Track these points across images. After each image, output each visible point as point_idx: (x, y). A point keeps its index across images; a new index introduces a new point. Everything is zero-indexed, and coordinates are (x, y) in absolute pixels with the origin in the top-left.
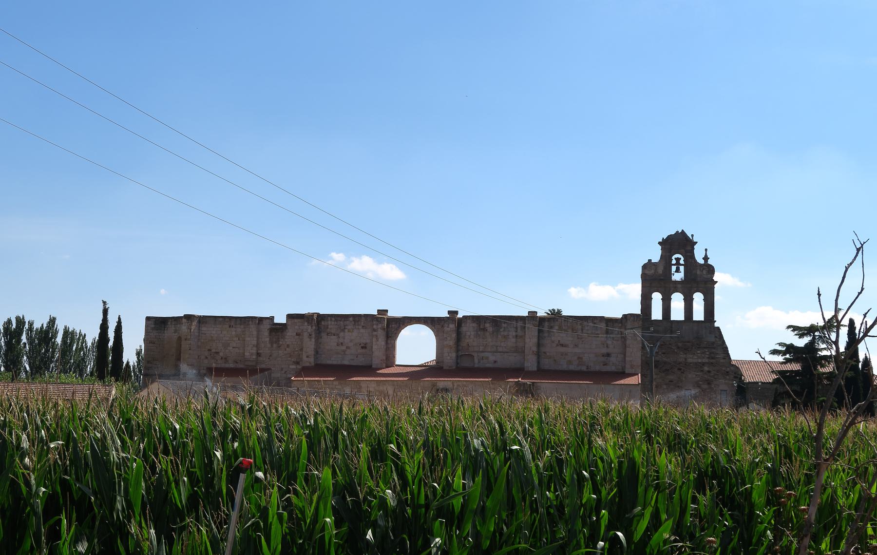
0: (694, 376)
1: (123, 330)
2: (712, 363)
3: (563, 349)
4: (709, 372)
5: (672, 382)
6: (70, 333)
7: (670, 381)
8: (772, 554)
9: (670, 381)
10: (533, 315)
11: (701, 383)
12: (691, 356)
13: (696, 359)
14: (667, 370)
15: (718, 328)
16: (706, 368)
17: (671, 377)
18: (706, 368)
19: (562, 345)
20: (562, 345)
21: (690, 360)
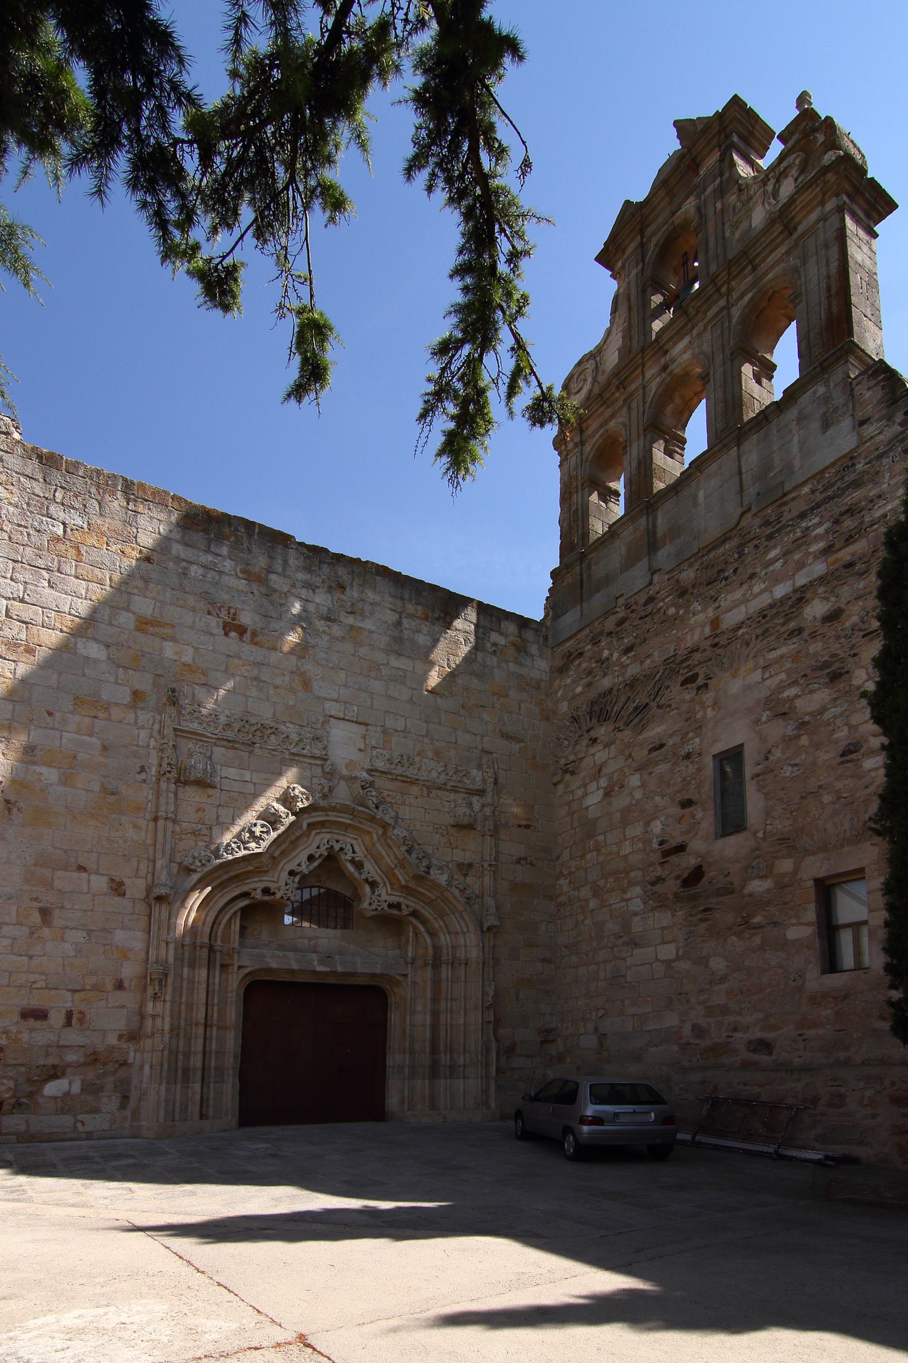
0: (757, 675)
1: (884, 186)
2: (850, 565)
3: (231, 1304)
4: (833, 616)
5: (662, 746)
6: (228, 539)
7: (652, 750)
8: (18, 782)
9: (652, 750)
10: (554, 574)
11: (792, 692)
12: (738, 595)
13: (762, 592)
14: (641, 709)
15: (872, 179)
16: (816, 609)
17: (655, 731)
18: (816, 609)
19: (11, 1339)
20: (11, 1339)
21: (730, 619)
